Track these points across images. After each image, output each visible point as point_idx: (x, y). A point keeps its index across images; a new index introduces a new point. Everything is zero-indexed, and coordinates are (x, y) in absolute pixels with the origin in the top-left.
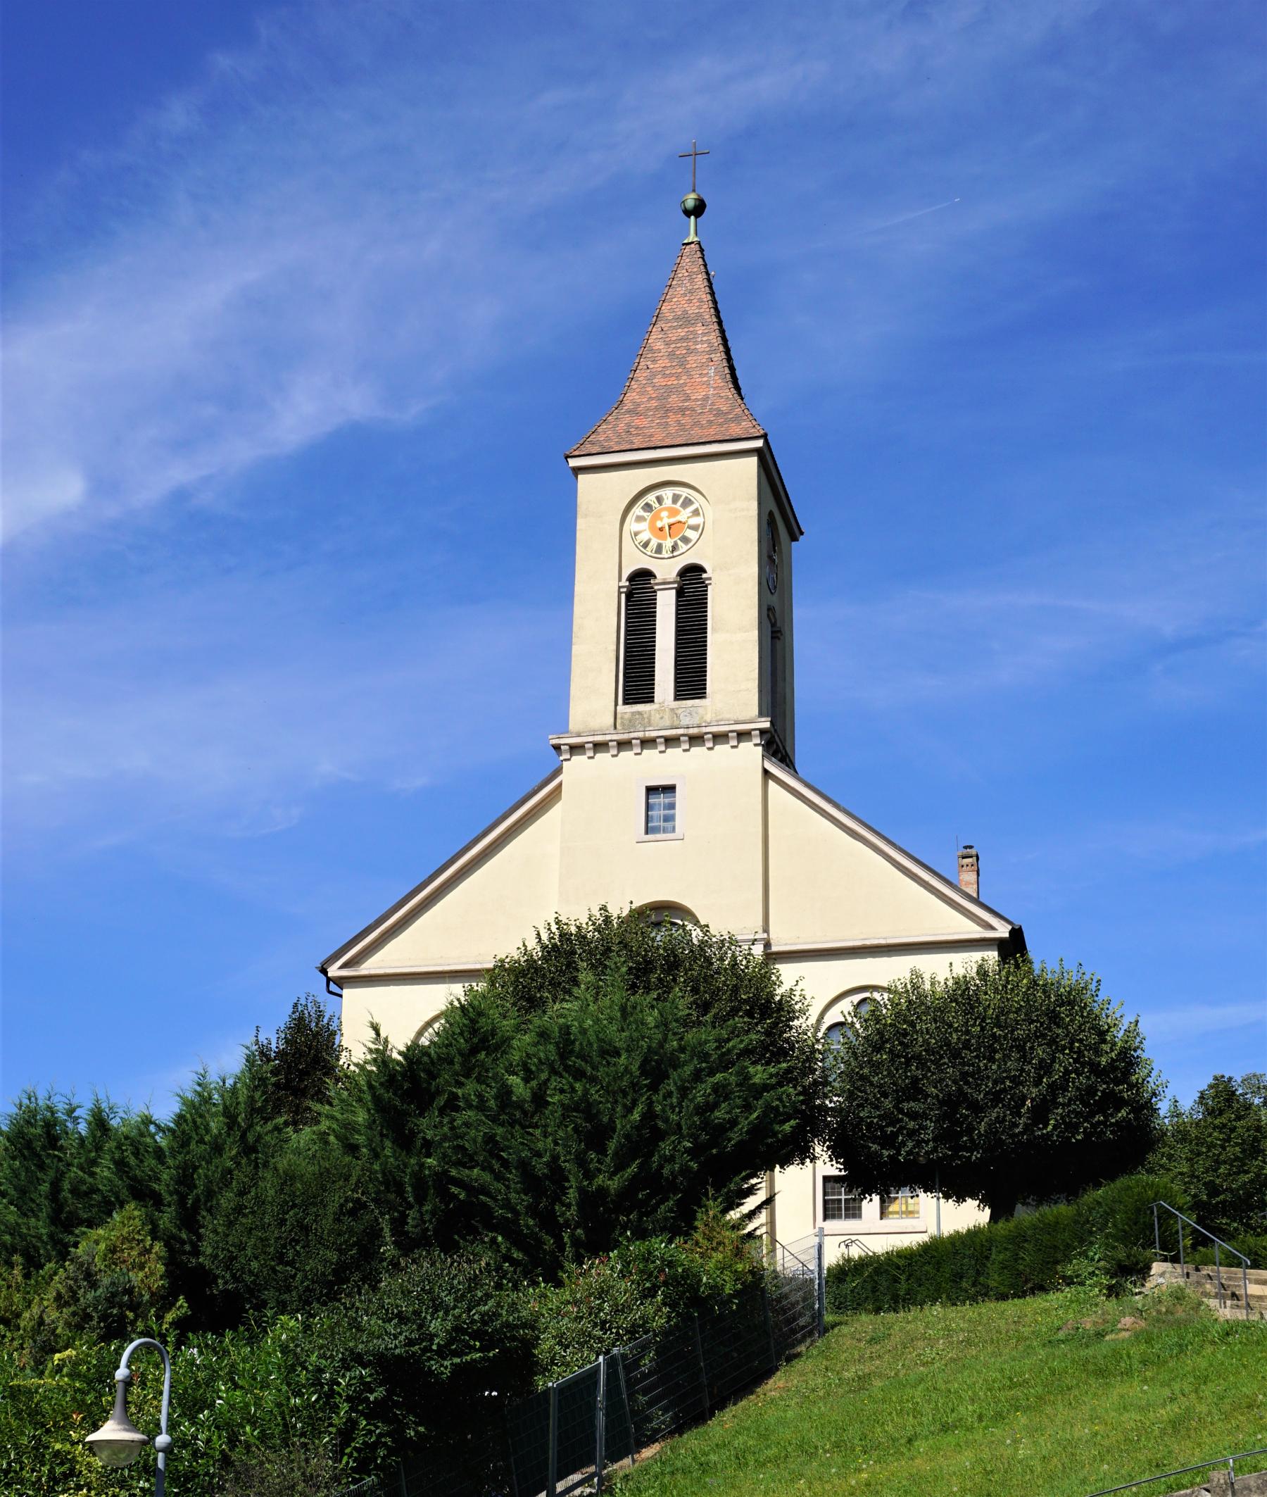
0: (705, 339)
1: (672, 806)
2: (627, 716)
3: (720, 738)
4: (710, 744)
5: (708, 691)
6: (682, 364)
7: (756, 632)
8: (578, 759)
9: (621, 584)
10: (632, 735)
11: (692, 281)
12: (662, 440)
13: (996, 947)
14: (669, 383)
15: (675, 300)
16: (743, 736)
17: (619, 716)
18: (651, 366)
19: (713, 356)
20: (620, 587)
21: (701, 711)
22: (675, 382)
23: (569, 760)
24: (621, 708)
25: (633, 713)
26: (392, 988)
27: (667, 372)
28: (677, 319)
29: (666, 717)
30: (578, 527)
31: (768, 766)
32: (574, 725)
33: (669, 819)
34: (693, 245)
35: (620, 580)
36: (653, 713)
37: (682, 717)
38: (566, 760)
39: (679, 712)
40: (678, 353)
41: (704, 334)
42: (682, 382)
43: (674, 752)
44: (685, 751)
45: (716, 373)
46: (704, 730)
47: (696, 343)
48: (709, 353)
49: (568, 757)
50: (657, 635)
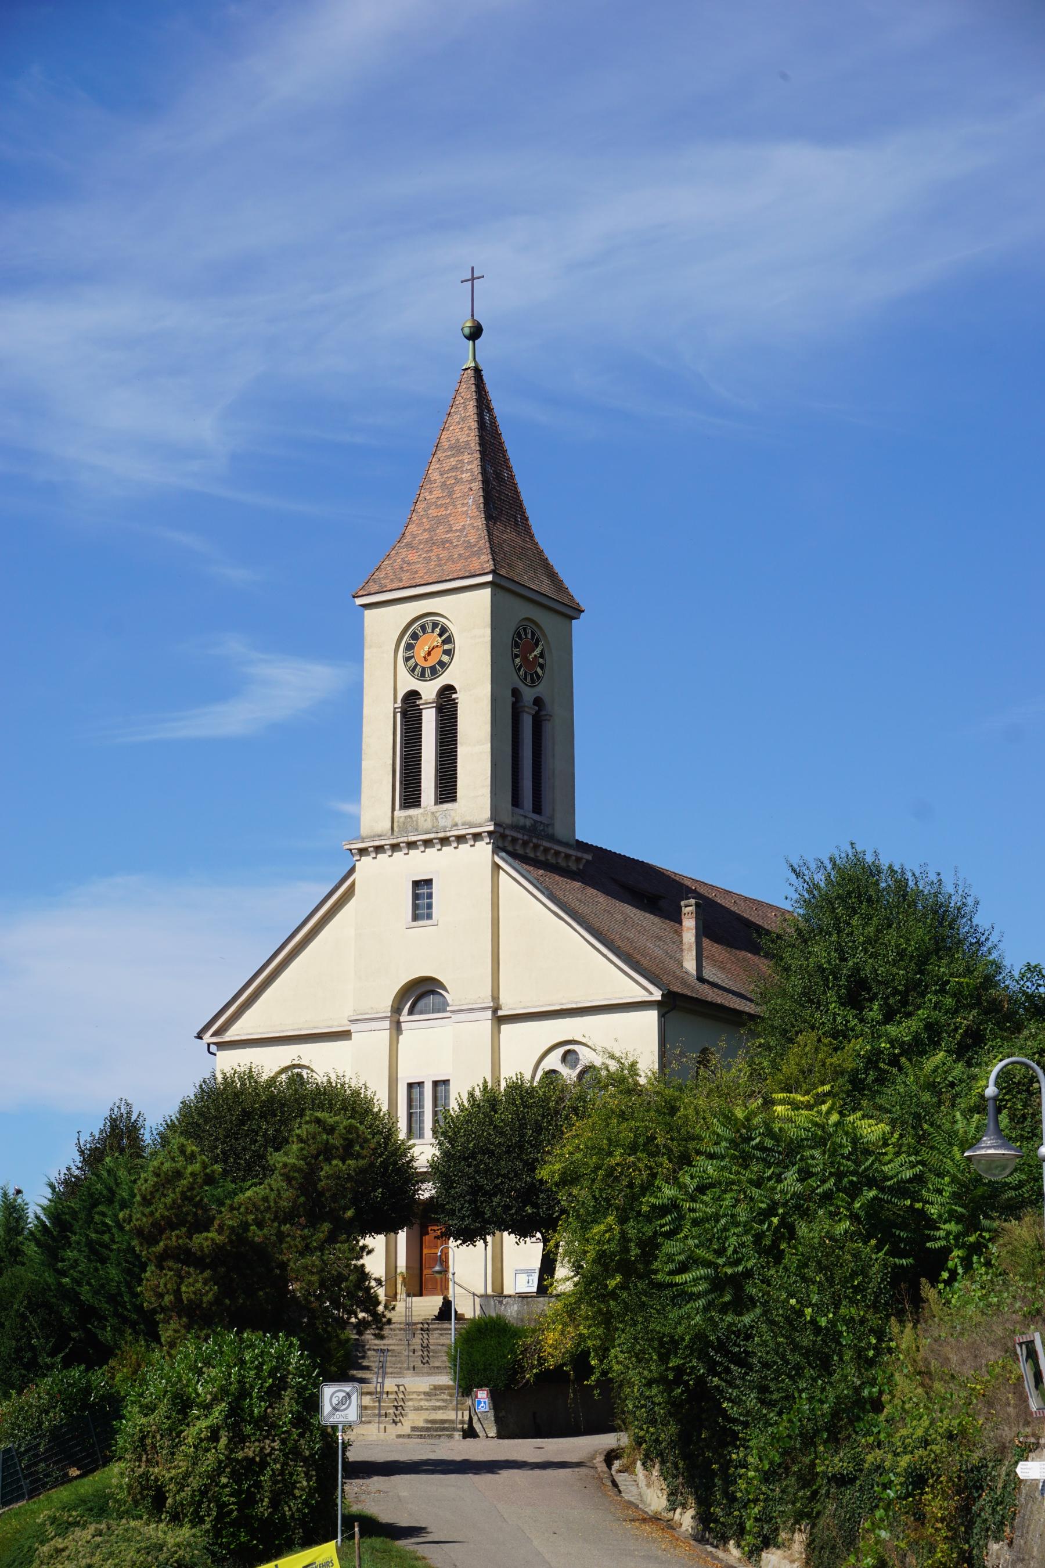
0: (469, 468)
1: (430, 896)
2: (402, 820)
3: (461, 839)
4: (455, 844)
5: (458, 794)
6: (450, 494)
7: (489, 745)
8: (366, 860)
9: (396, 706)
10: (400, 840)
11: (465, 408)
12: (422, 577)
13: (656, 1007)
14: (439, 514)
15: (451, 428)
16: (477, 837)
17: (396, 820)
18: (428, 498)
19: (472, 485)
20: (395, 708)
21: (452, 813)
22: (444, 513)
23: (359, 860)
24: (398, 813)
25: (406, 817)
26: (248, 1050)
27: (439, 503)
28: (451, 448)
29: (429, 820)
30: (365, 657)
31: (497, 860)
32: (365, 830)
33: (430, 906)
34: (469, 371)
35: (395, 702)
36: (419, 816)
37: (440, 820)
38: (357, 860)
39: (437, 814)
40: (448, 483)
41: (469, 463)
42: (448, 512)
43: (431, 852)
44: (439, 850)
45: (474, 501)
46: (449, 834)
47: (462, 472)
48: (471, 482)
49: (358, 858)
50: (423, 747)
